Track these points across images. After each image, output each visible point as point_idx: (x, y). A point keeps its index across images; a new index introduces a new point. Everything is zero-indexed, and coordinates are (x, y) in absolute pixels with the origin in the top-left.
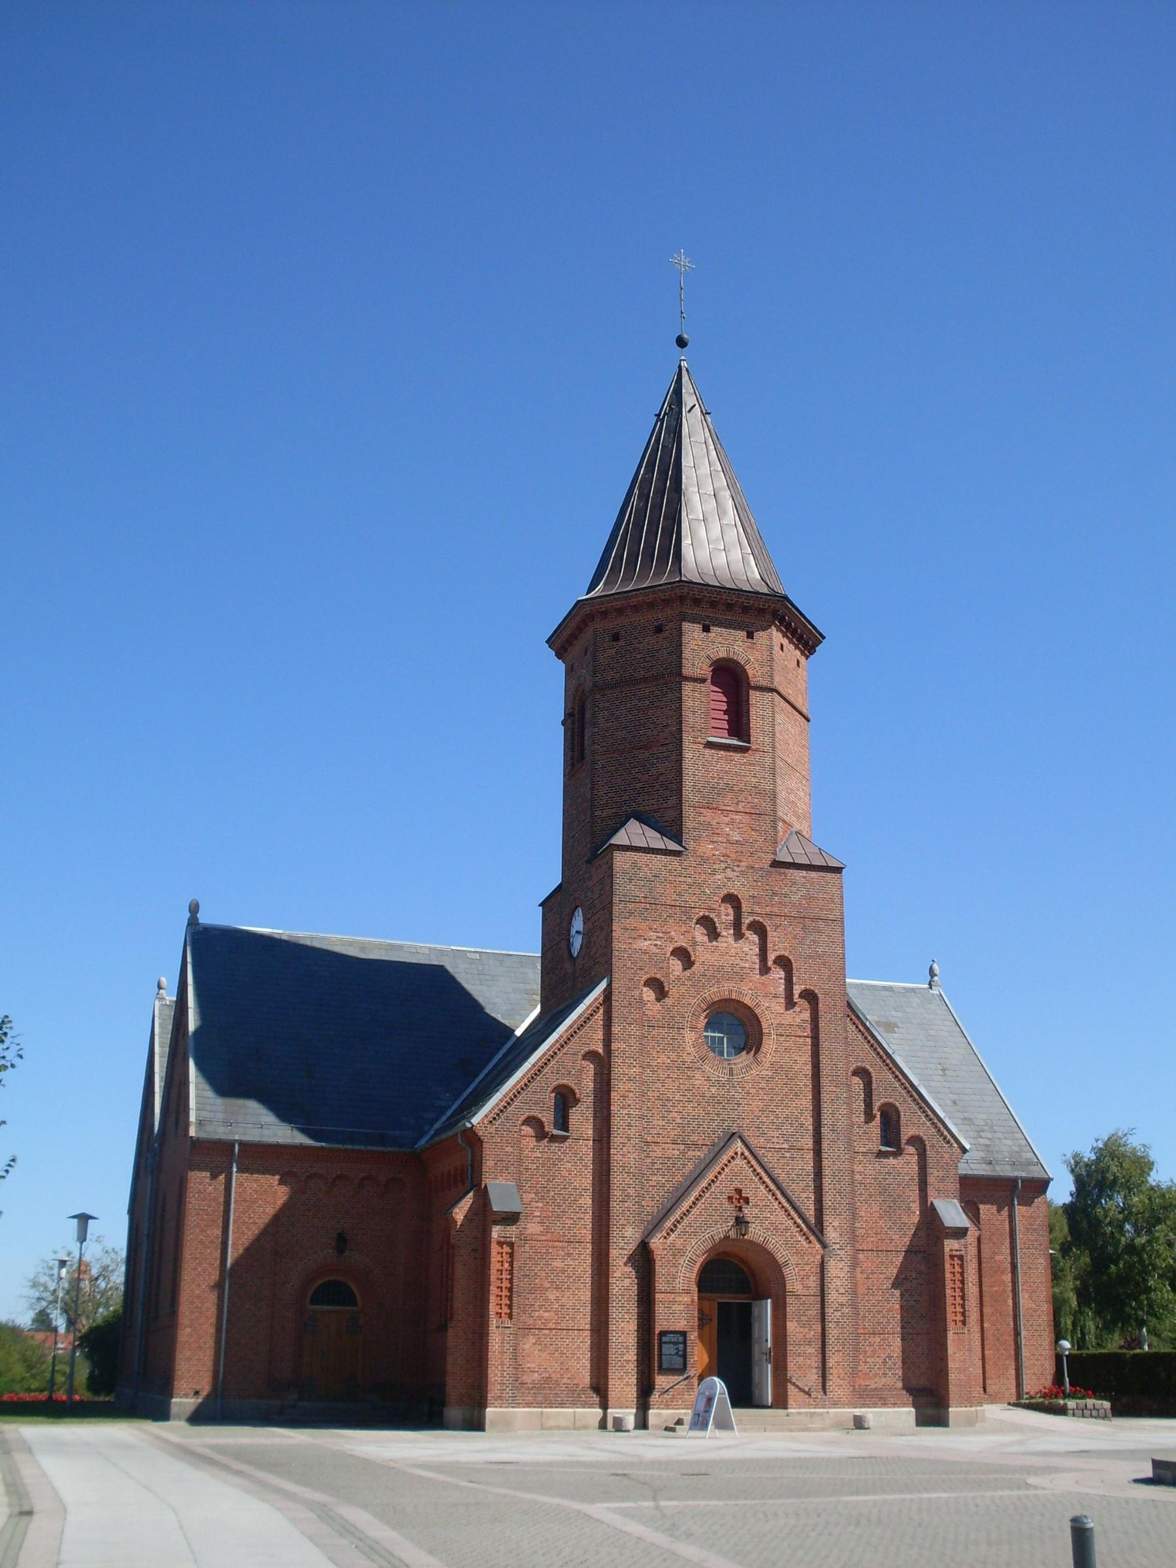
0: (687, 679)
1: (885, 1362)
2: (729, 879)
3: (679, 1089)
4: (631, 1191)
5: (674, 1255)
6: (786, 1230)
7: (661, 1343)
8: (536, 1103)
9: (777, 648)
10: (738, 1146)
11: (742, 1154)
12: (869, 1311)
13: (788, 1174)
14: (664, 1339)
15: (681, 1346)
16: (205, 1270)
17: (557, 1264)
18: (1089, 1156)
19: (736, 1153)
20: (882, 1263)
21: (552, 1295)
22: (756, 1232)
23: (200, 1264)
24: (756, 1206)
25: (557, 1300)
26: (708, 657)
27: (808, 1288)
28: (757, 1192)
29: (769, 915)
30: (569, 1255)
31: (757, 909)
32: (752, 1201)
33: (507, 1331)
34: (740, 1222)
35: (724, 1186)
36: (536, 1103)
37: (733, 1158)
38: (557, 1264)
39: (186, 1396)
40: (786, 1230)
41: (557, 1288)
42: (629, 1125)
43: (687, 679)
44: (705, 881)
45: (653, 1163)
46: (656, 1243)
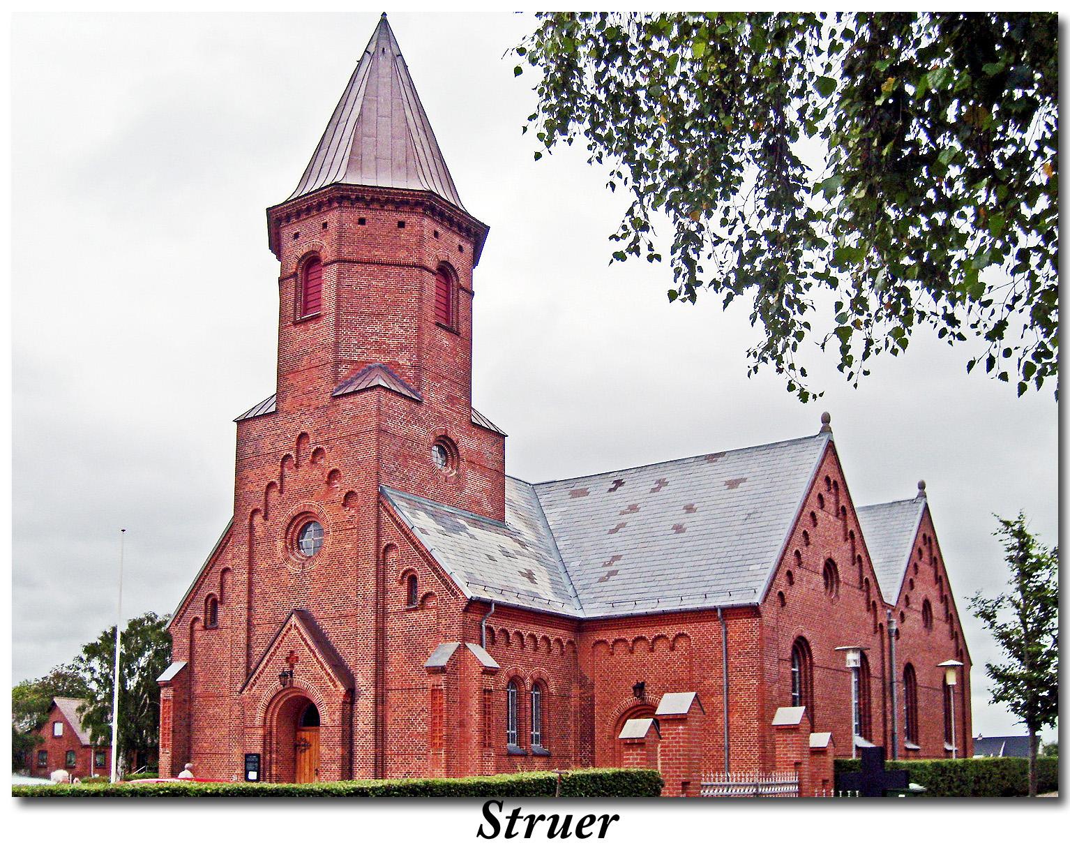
11: (295, 625)
12: (395, 737)
17: (210, 712)
27: (334, 721)
30: (217, 705)
38: (210, 712)
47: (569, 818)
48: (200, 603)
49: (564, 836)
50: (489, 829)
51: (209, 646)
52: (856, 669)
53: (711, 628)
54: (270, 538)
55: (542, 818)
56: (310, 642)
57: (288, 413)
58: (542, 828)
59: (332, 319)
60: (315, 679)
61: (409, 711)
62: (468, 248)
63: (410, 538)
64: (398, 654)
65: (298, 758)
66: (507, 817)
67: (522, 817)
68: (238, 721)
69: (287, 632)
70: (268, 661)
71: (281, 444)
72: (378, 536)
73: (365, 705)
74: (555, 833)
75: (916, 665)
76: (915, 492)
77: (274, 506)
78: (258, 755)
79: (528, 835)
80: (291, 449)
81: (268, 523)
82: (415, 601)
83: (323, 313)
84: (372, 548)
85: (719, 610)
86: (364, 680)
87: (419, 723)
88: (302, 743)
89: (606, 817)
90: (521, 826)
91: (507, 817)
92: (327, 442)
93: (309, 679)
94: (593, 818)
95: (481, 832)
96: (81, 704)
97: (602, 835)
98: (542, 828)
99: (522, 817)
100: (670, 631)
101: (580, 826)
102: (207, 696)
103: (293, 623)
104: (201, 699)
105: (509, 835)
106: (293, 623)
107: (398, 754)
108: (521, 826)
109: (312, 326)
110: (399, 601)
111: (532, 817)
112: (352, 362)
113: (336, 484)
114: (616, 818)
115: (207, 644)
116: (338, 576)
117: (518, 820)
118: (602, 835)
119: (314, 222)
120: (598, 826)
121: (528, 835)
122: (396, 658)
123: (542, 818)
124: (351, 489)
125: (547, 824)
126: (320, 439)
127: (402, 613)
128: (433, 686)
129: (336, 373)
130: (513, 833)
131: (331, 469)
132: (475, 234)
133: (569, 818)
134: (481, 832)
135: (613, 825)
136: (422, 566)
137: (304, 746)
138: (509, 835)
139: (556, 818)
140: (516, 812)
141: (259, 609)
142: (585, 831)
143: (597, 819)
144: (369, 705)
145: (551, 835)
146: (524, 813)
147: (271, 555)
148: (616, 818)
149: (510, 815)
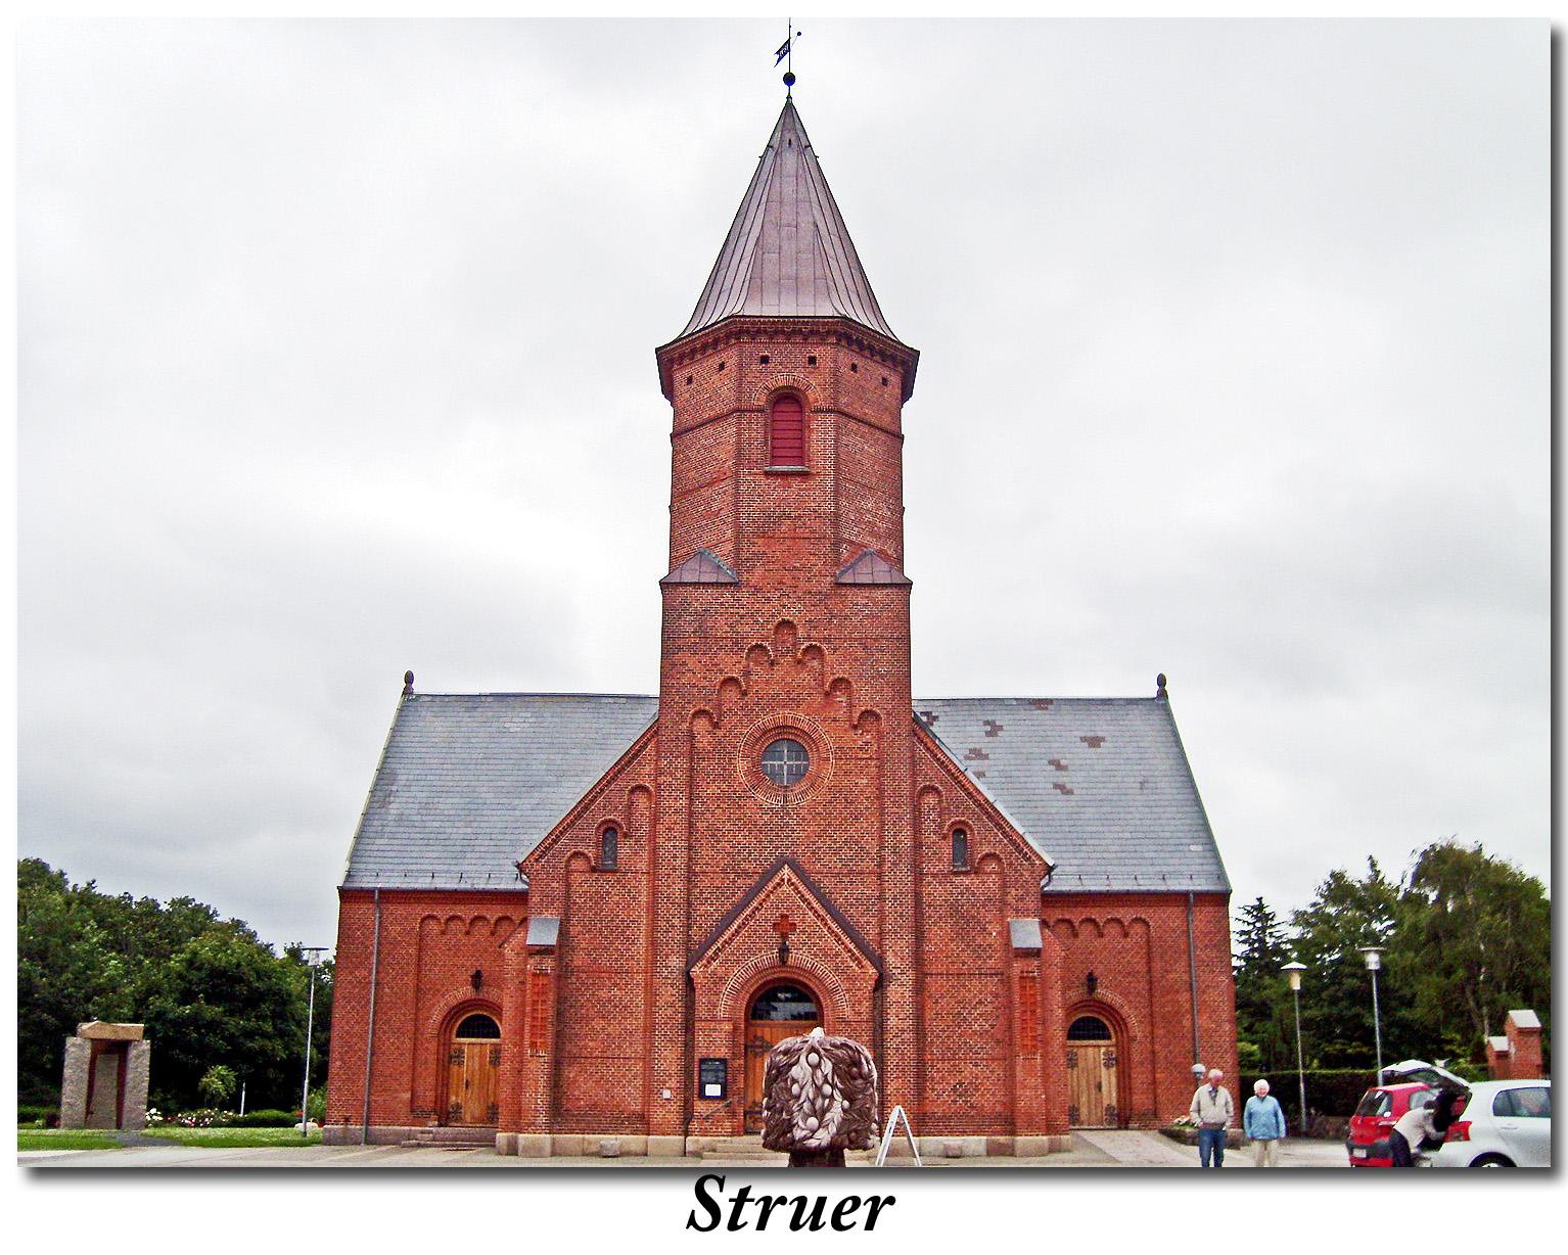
0: (760, 410)
1: (954, 1089)
2: (784, 606)
3: (729, 819)
4: (676, 922)
5: (715, 983)
6: (837, 955)
7: (700, 1071)
8: (583, 839)
9: (845, 370)
10: (786, 871)
11: (789, 880)
12: (938, 1037)
13: (846, 899)
14: (704, 1067)
15: (721, 1074)
16: (353, 1008)
17: (603, 994)
18: (1486, 855)
19: (783, 880)
20: (953, 987)
21: (598, 1024)
22: (800, 957)
23: (349, 1002)
24: (804, 932)
25: (603, 1029)
26: (766, 388)
27: (860, 1014)
28: (807, 917)
29: (827, 640)
30: (615, 985)
31: (814, 634)
32: (800, 927)
33: (542, 1060)
34: (784, 951)
35: (768, 914)
36: (583, 839)
37: (778, 884)
38: (603, 994)
39: (337, 1123)
40: (837, 955)
41: (603, 1018)
42: (675, 857)
43: (760, 410)
44: (758, 610)
45: (701, 893)
46: (696, 970)
47: (821, 1201)
48: (590, 828)
49: (815, 1227)
50: (704, 1217)
51: (599, 898)
52: (1376, 971)
53: (1171, 916)
54: (724, 751)
55: (782, 1200)
56: (815, 905)
57: (758, 590)
58: (782, 1215)
59: (830, 483)
60: (826, 955)
61: (959, 1002)
62: (895, 380)
63: (959, 782)
64: (941, 928)
65: (750, 1064)
66: (731, 1200)
67: (752, 1200)
68: (670, 1011)
69: (775, 888)
70: (739, 927)
71: (747, 629)
72: (914, 775)
73: (899, 992)
74: (801, 1223)
75: (1096, 973)
76: (1152, 691)
77: (730, 710)
78: (723, 1061)
79: (761, 1226)
80: (766, 638)
81: (720, 733)
82: (966, 861)
83: (814, 472)
84: (906, 787)
85: (1191, 895)
86: (897, 958)
87: (976, 1020)
88: (758, 1043)
89: (875, 1200)
90: (751, 1213)
91: (731, 1200)
92: (827, 640)
93: (816, 955)
94: (856, 1201)
95: (692, 1222)
96: (1453, 977)
97: (870, 1226)
98: (782, 1215)
99: (752, 1200)
100: (1126, 914)
101: (838, 1212)
102: (596, 971)
103: (786, 877)
104: (585, 975)
105: (733, 1226)
106: (786, 877)
107: (943, 1060)
108: (751, 1213)
109: (795, 483)
110: (939, 860)
111: (767, 1200)
112: (852, 542)
113: (837, 696)
114: (891, 1200)
115: (597, 893)
116: (845, 819)
117: (747, 1204)
118: (870, 1226)
119: (800, 354)
120: (863, 1212)
121: (761, 1226)
122: (938, 934)
123: (782, 1200)
124: (869, 708)
125: (789, 1210)
126: (814, 634)
127: (945, 876)
128: (1022, 972)
129: (838, 554)
130: (739, 1223)
131: (836, 676)
132: (903, 363)
133: (821, 1201)
134: (692, 1222)
135: (886, 1211)
136: (979, 819)
137: (761, 1047)
138: (733, 1226)
139: (802, 1201)
140: (744, 1193)
141: (705, 852)
142: (845, 1220)
143: (862, 1202)
144: (907, 994)
145: (795, 1225)
146: (756, 1193)
147: (726, 775)
148: (891, 1200)
149: (735, 1196)
